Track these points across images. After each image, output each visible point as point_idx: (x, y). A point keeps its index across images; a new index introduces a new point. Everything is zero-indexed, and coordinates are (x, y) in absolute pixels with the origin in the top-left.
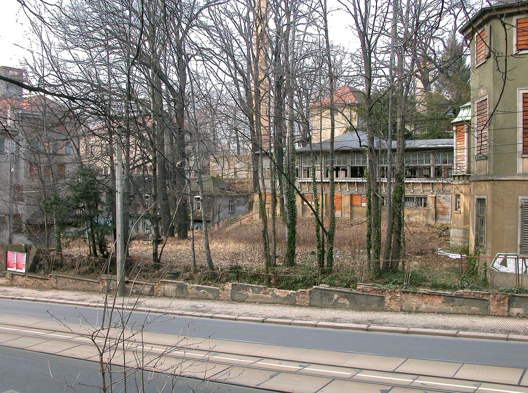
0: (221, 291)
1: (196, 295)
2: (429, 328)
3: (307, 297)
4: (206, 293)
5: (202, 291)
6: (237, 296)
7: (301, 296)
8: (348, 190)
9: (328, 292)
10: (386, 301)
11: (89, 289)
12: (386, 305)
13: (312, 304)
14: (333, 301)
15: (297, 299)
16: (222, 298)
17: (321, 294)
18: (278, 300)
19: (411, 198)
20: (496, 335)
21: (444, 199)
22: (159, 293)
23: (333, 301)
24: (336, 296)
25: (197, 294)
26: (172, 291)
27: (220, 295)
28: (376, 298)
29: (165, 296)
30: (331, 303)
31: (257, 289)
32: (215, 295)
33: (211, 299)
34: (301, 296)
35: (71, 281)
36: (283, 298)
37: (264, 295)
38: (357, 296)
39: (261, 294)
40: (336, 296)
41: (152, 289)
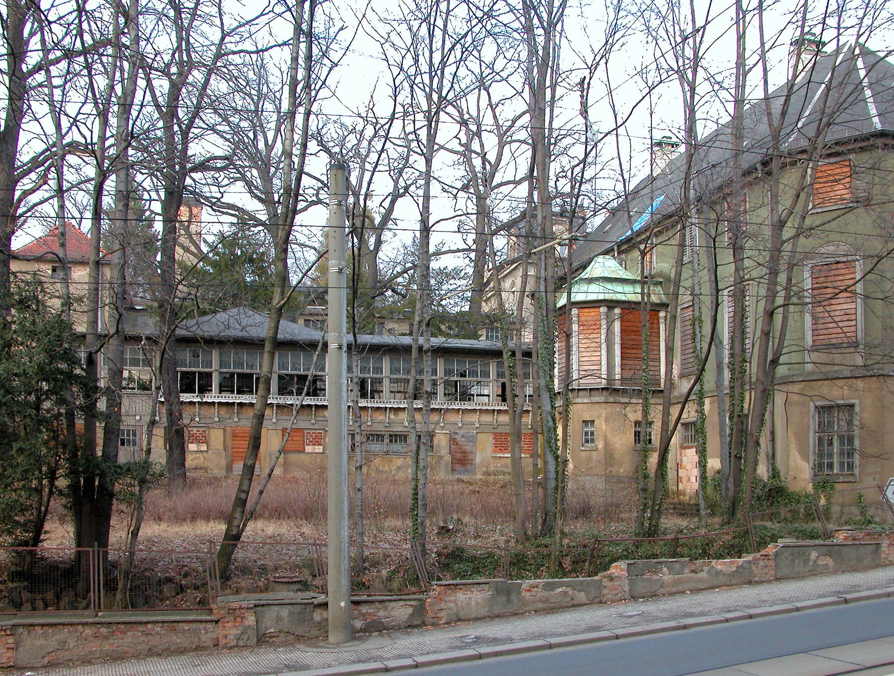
0: (606, 582)
1: (543, 602)
2: (734, 611)
3: (772, 563)
4: (571, 592)
5: (560, 590)
6: (641, 587)
7: (761, 563)
8: (274, 420)
9: (803, 549)
10: (883, 549)
11: (173, 648)
12: (883, 556)
13: (780, 575)
14: (811, 563)
15: (756, 572)
16: (610, 596)
17: (792, 554)
18: (722, 579)
19: (400, 436)
20: (876, 592)
21: (463, 436)
22: (443, 614)
23: (811, 563)
24: (814, 555)
25: (547, 600)
26: (477, 603)
27: (605, 591)
28: (869, 547)
29: (459, 620)
30: (807, 569)
31: (677, 566)
32: (593, 593)
33: (586, 604)
34: (761, 563)
35: (88, 631)
36: (729, 575)
37: (693, 575)
38: (845, 550)
39: (687, 574)
40: (814, 555)
41: (421, 609)
